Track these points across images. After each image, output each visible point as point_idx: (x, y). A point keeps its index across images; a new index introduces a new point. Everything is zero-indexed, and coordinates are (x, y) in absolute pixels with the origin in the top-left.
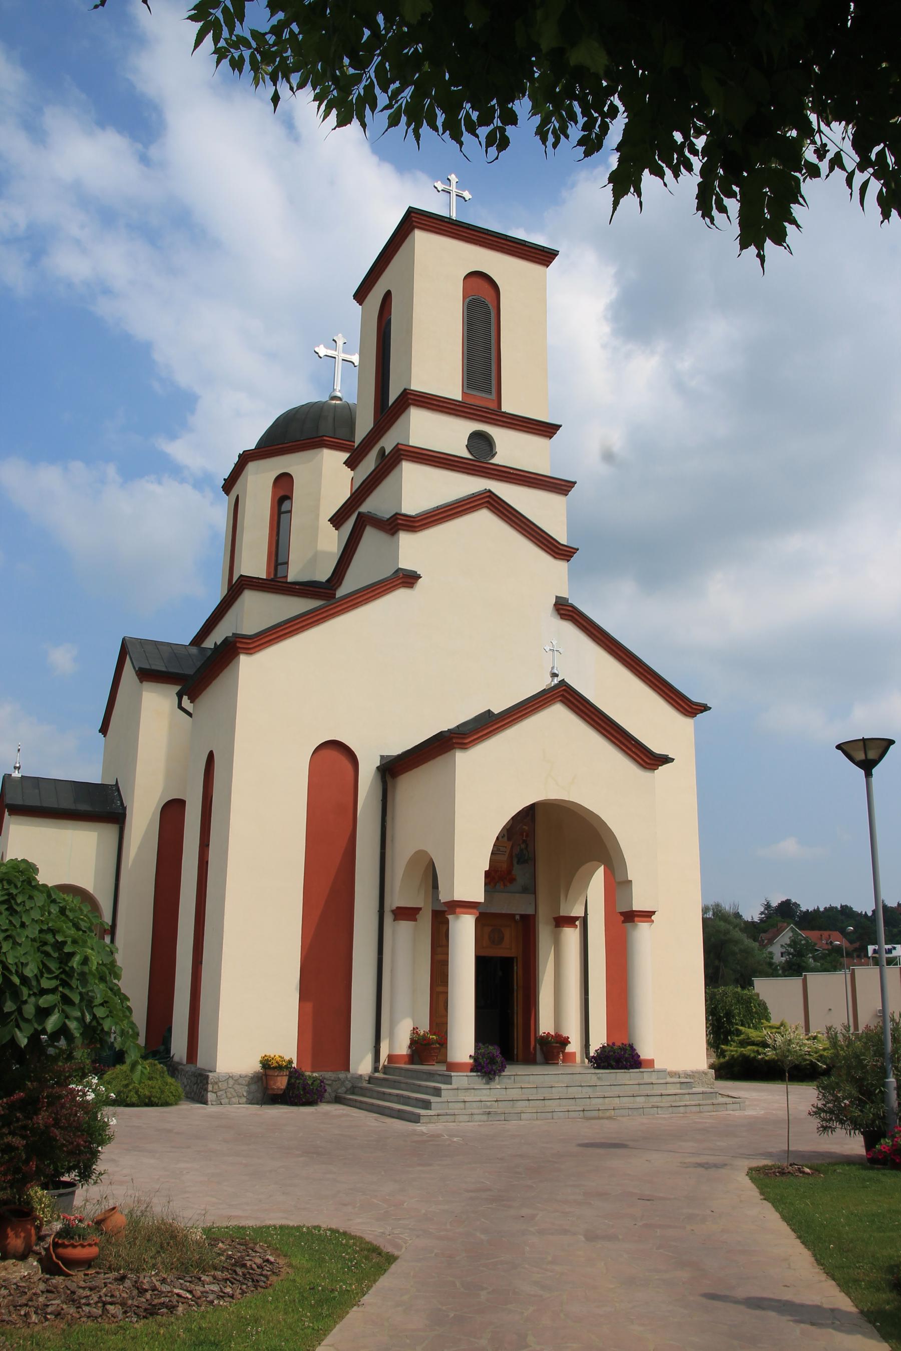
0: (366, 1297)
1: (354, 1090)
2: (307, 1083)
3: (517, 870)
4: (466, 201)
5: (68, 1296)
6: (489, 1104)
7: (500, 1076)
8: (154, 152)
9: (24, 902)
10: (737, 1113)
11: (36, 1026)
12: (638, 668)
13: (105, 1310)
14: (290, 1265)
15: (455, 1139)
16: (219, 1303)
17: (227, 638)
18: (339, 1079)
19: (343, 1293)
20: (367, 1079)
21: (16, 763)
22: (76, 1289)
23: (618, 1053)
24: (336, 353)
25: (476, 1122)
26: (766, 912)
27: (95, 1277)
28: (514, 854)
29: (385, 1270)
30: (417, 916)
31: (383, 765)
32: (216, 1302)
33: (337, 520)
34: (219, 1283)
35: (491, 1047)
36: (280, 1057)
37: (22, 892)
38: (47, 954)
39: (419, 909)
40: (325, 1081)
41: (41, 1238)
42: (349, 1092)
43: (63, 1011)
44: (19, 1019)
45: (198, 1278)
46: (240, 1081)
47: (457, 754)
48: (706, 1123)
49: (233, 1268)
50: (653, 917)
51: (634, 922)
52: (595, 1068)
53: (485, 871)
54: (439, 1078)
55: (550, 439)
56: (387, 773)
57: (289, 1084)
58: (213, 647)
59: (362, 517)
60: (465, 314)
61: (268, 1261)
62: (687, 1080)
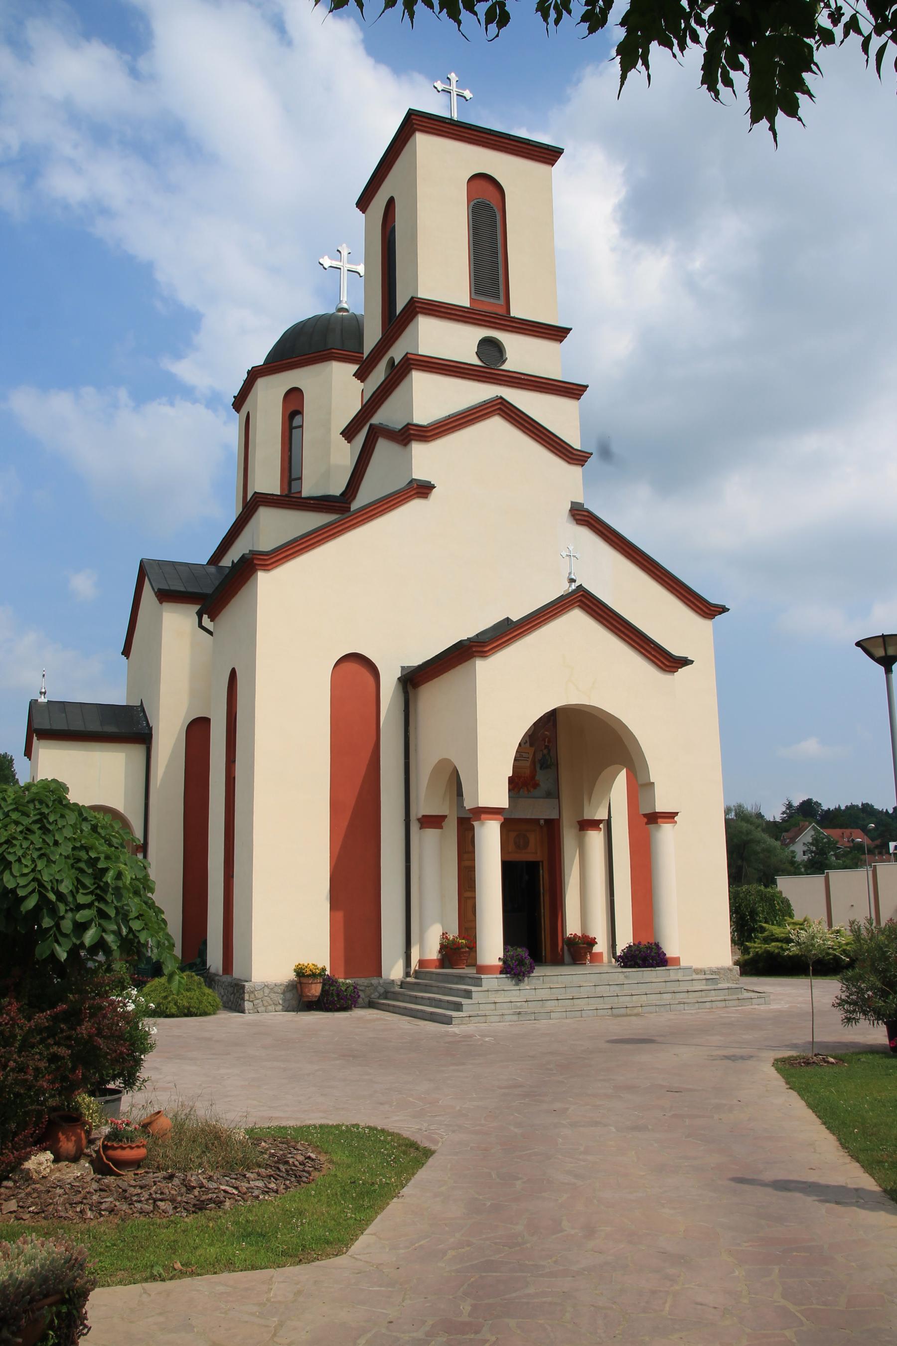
1: (386, 995)
2: (341, 989)
4: (467, 100)
5: (120, 1194)
6: (519, 1004)
7: (529, 977)
8: (142, 64)
9: (56, 821)
10: (762, 1007)
11: (74, 940)
13: (156, 1207)
14: (331, 1161)
15: (487, 1039)
16: (264, 1197)
17: (243, 555)
18: (372, 985)
20: (399, 983)
21: (42, 688)
29: (423, 1164)
32: (261, 1197)
33: (349, 433)
35: (519, 950)
36: (313, 965)
38: (81, 871)
40: (358, 987)
41: (91, 1142)
43: (100, 925)
45: (243, 1176)
46: (276, 989)
50: (676, 818)
51: (657, 823)
52: (622, 967)
56: (409, 683)
57: (323, 990)
59: (374, 429)
61: (309, 1158)
62: (713, 976)
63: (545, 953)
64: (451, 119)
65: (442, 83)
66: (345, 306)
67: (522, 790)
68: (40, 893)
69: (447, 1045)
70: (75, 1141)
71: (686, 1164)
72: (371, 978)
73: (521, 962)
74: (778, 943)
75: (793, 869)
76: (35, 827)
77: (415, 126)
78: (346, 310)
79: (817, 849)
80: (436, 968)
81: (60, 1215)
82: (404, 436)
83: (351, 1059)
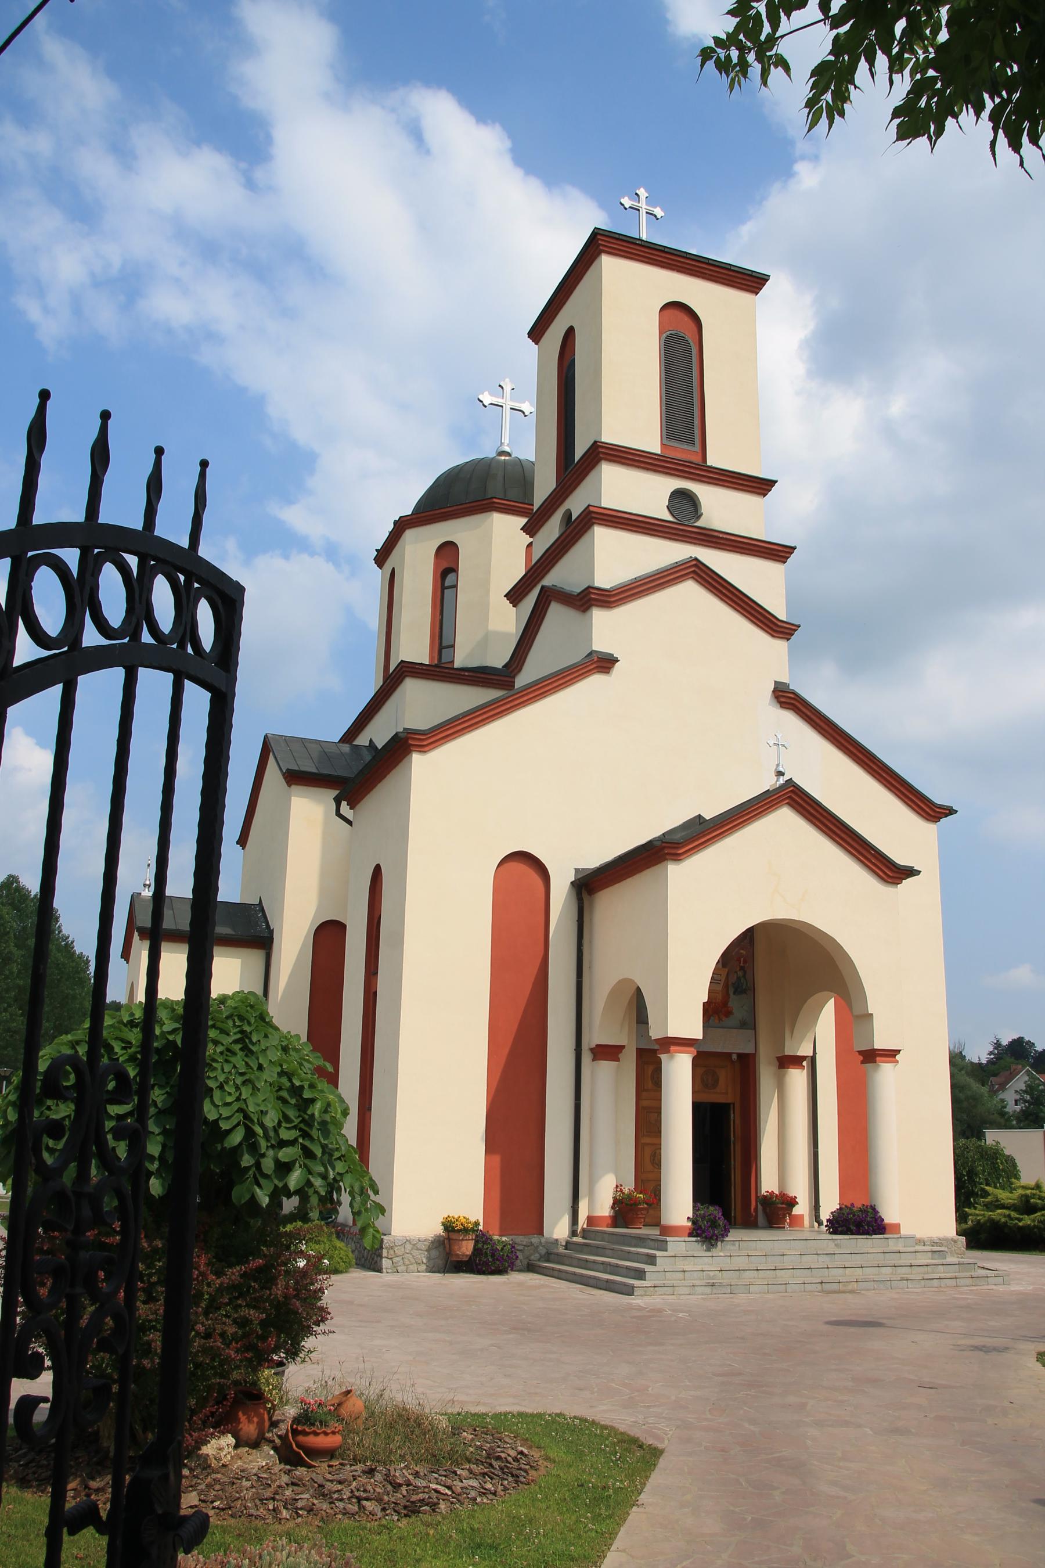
0: (642, 1496)
1: (549, 1256)
2: (497, 1248)
3: (734, 1002)
4: (657, 219)
5: (316, 1490)
6: (712, 1274)
7: (722, 1241)
8: (259, 174)
9: (259, 1041)
10: (1001, 1288)
11: (276, 1182)
12: (871, 765)
13: (362, 1508)
14: (547, 1458)
15: (680, 1315)
16: (482, 1500)
17: (397, 734)
18: (532, 1244)
19: (617, 1490)
20: (564, 1244)
21: (146, 880)
22: (324, 1483)
23: (858, 1216)
24: (503, 401)
25: (698, 1295)
26: (996, 1051)
27: (341, 1469)
28: (730, 983)
29: (655, 1465)
30: (620, 1056)
31: (579, 879)
32: (479, 1500)
33: (515, 596)
34: (477, 1477)
35: (711, 1208)
36: (464, 1218)
37: (257, 1030)
38: (284, 1101)
39: (622, 1047)
40: (516, 1246)
41: (274, 1424)
42: (543, 1259)
43: (305, 1166)
44: (258, 1176)
45: (453, 1472)
46: (420, 1245)
47: (669, 866)
48: (968, 1298)
49: (488, 1460)
50: (897, 1057)
51: (875, 1062)
52: (831, 1233)
53: (704, 1003)
54: (651, 1243)
55: (764, 496)
56: (583, 890)
57: (475, 1249)
58: (368, 745)
59: (546, 591)
60: (663, 352)
61: (522, 1453)
62: (937, 1247)
63: (735, 1213)
64: (639, 239)
65: (630, 199)
66: (507, 449)
67: (712, 1018)
68: (245, 1125)
69: (634, 1320)
70: (257, 1422)
71: (973, 1479)
72: (531, 1236)
73: (714, 1224)
74: (1004, 1211)
75: (1004, 1122)
76: (237, 1047)
77: (601, 248)
78: (509, 454)
79: (1032, 1098)
80: (607, 1227)
81: (250, 1514)
82: (584, 601)
83: (526, 1333)
